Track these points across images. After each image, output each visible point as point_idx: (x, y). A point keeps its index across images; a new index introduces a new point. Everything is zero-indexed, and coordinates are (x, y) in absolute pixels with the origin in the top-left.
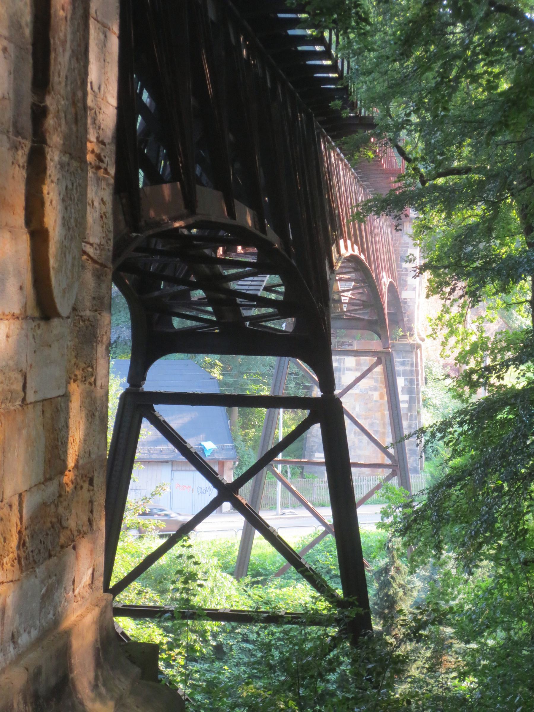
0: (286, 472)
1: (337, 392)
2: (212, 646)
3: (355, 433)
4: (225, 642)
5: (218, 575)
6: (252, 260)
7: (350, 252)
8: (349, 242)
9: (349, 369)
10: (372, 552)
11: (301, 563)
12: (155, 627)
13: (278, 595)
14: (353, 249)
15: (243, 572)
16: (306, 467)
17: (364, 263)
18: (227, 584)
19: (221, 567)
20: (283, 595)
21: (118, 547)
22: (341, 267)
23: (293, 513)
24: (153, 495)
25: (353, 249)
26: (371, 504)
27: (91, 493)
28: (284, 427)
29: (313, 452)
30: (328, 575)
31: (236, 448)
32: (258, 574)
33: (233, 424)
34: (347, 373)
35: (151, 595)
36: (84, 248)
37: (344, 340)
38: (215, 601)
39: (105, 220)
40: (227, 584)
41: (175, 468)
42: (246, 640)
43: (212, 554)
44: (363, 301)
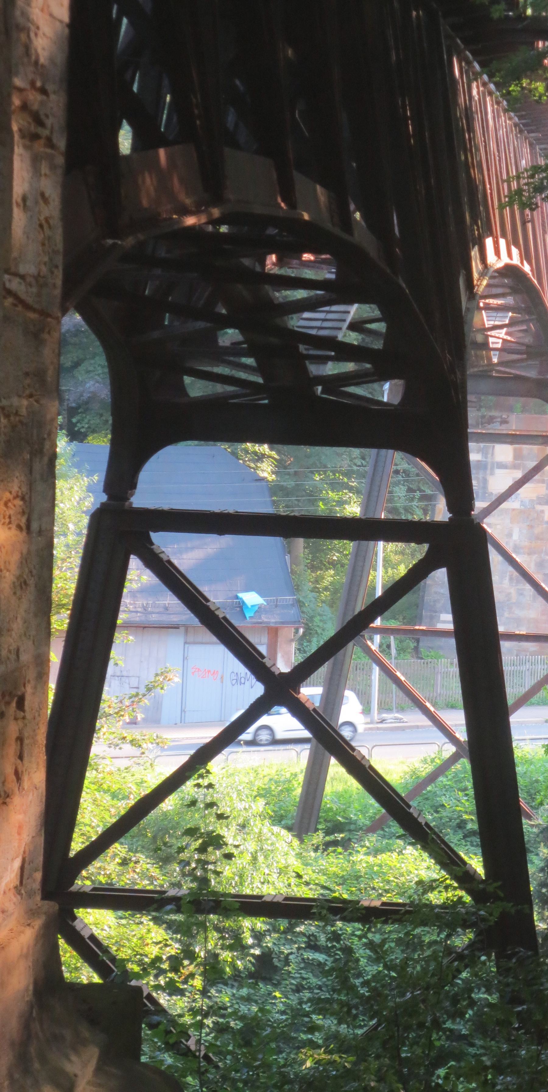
0: (389, 646)
1: (479, 505)
2: (253, 955)
3: (511, 579)
4: (276, 949)
5: (265, 830)
6: (329, 274)
7: (505, 260)
8: (502, 242)
9: (502, 466)
10: (539, 792)
11: (411, 814)
12: (151, 923)
13: (370, 867)
14: (510, 255)
15: (309, 824)
16: (422, 638)
17: (529, 280)
18: (282, 846)
19: (271, 817)
20: (380, 866)
21: (86, 782)
22: (488, 286)
23: (400, 720)
24: (149, 690)
25: (510, 255)
26: (538, 704)
27: (20, 722)
28: (384, 566)
29: (436, 612)
30: (460, 832)
31: (299, 604)
32: (336, 827)
33: (294, 561)
34: (499, 472)
35: (145, 866)
36: (8, 285)
37: (493, 413)
38: (258, 877)
39: (47, 232)
40: (282, 846)
41: (190, 639)
42: (313, 945)
43: (255, 793)
44: (528, 346)
